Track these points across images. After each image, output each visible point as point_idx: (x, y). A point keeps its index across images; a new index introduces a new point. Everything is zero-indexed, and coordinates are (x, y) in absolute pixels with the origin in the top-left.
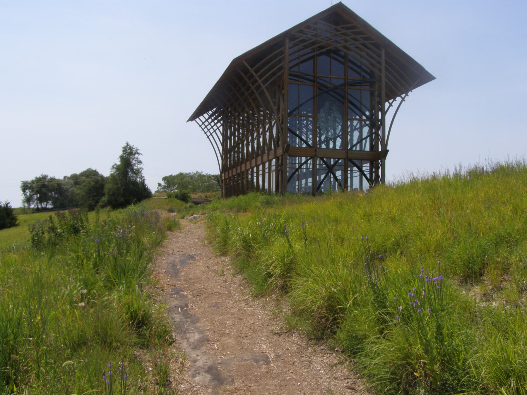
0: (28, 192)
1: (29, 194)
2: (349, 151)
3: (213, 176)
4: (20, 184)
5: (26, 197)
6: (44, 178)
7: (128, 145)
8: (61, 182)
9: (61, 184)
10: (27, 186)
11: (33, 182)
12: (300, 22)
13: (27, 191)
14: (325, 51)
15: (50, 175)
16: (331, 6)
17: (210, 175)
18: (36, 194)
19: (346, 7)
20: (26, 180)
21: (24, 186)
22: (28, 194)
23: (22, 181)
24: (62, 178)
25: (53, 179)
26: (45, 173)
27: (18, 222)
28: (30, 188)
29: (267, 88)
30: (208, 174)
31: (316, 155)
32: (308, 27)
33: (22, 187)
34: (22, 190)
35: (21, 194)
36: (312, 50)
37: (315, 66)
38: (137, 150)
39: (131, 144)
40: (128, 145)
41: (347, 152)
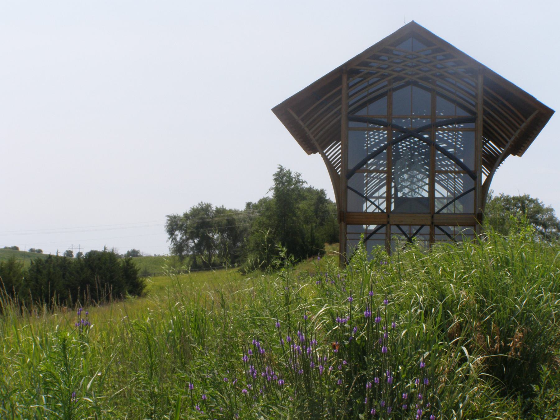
0: (179, 235)
1: (181, 239)
2: (435, 216)
3: (514, 198)
4: (164, 222)
5: (175, 244)
6: (206, 209)
7: (281, 169)
8: (235, 217)
9: (234, 220)
10: (177, 225)
11: (186, 216)
12: (357, 54)
13: (177, 232)
14: (403, 84)
15: (215, 204)
16: (404, 25)
17: (508, 196)
18: (192, 238)
19: (286, 100)
20: (175, 214)
21: (171, 225)
22: (178, 239)
23: (168, 216)
24: (242, 207)
25: (220, 211)
26: (206, 201)
27: (144, 291)
28: (180, 228)
29: (317, 141)
30: (505, 195)
31: (388, 222)
32: (366, 64)
33: (169, 226)
34: (168, 231)
35: (167, 239)
36: (443, 58)
37: (390, 105)
38: (298, 176)
39: (286, 168)
40: (281, 169)
41: (432, 217)
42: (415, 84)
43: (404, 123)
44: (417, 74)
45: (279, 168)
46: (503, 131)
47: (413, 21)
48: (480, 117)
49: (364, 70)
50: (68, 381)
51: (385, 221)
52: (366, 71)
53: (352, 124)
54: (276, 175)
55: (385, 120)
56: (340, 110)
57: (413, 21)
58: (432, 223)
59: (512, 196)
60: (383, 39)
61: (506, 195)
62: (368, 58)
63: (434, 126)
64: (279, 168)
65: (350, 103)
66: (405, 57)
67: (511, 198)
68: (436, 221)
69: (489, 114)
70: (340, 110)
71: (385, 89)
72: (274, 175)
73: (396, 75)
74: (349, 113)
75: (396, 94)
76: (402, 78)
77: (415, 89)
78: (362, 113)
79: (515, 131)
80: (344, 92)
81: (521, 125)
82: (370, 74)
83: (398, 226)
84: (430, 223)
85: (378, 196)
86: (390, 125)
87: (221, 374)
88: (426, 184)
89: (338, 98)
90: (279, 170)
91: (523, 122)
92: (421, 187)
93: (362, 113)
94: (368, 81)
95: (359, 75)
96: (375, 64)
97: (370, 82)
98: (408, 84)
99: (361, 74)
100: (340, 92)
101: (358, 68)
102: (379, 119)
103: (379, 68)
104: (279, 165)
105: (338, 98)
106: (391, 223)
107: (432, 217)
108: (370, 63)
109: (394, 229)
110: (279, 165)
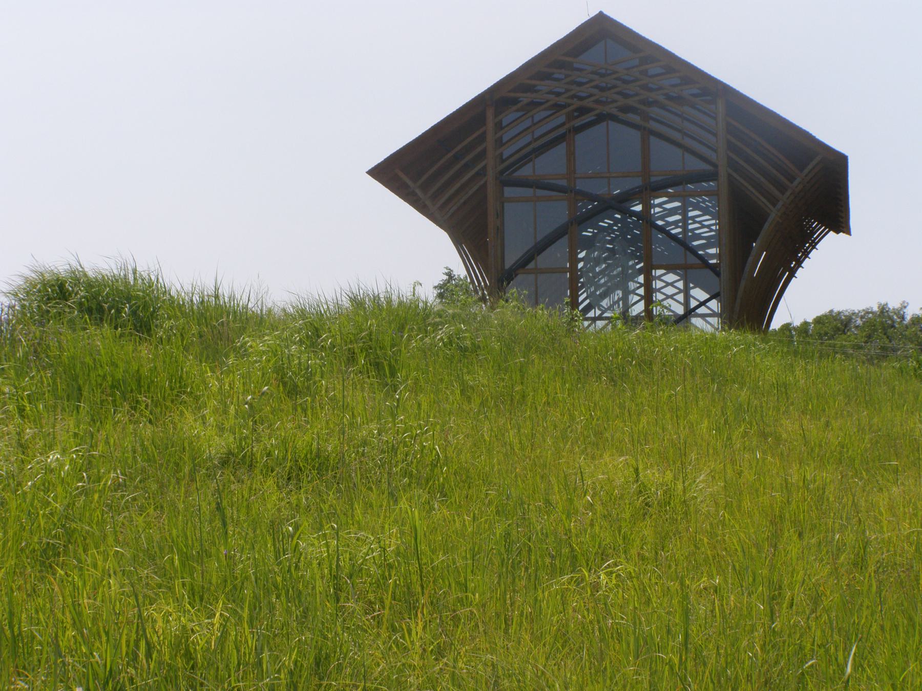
14: (593, 118)
16: (589, 18)
32: (561, 65)
37: (571, 155)
42: (612, 117)
43: (599, 189)
44: (614, 101)
45: (446, 274)
47: (601, 13)
48: (723, 171)
49: (525, 98)
52: (526, 101)
53: (509, 192)
54: (439, 287)
55: (563, 183)
57: (601, 13)
60: (501, 80)
62: (510, 92)
63: (646, 189)
64: (446, 274)
65: (506, 154)
66: (592, 73)
71: (562, 131)
72: (435, 287)
73: (577, 103)
74: (502, 172)
75: (579, 138)
76: (588, 110)
77: (613, 125)
78: (526, 172)
80: (490, 137)
82: (534, 104)
85: (593, 316)
86: (571, 191)
89: (479, 149)
90: (446, 277)
92: (671, 297)
93: (526, 172)
94: (532, 117)
95: (515, 108)
96: (544, 86)
97: (537, 119)
98: (601, 118)
99: (519, 105)
100: (482, 138)
101: (513, 95)
102: (546, 181)
103: (550, 92)
104: (447, 268)
105: (479, 149)
108: (553, 74)
110: (447, 268)
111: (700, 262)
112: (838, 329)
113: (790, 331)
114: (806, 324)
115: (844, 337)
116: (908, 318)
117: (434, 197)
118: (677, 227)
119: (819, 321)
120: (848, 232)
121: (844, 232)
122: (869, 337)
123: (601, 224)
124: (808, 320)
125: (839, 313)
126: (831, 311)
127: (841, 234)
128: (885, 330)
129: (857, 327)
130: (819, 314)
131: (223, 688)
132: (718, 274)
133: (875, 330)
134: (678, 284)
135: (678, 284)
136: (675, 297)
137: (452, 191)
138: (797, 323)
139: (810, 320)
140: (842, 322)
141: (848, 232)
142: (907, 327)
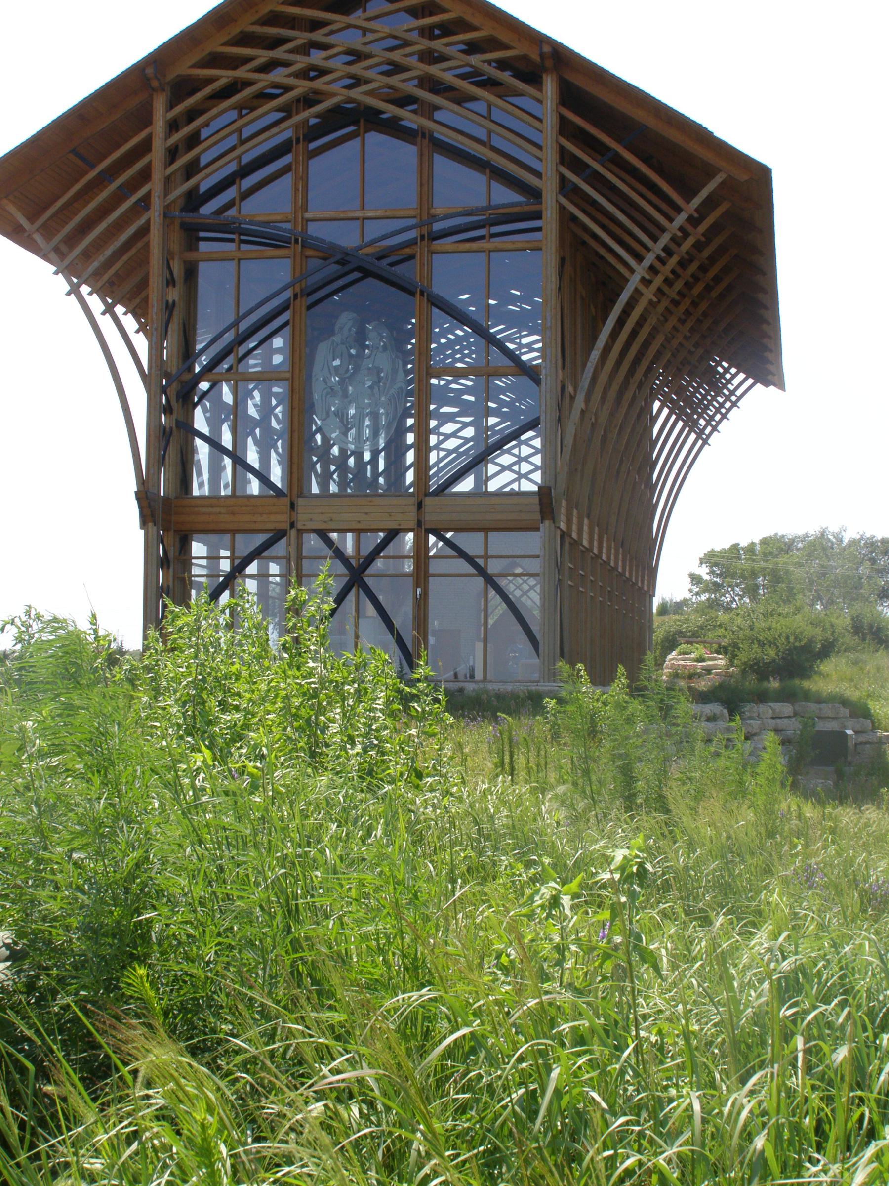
31: (292, 525)
46: (621, 242)
50: (608, 1116)
51: (281, 520)
56: (148, 195)
58: (419, 524)
59: (879, 539)
61: (868, 536)
67: (876, 541)
68: (431, 517)
69: (576, 189)
70: (148, 195)
79: (655, 239)
81: (671, 220)
83: (323, 534)
84: (413, 524)
87: (588, 1057)
88: (537, 468)
91: (679, 210)
106: (300, 526)
107: (420, 505)
109: (312, 541)
111: (513, 364)
112: (782, 550)
113: (738, 551)
114: (753, 544)
115: (787, 556)
116: (846, 541)
117: (71, 240)
118: (532, 350)
119: (764, 542)
120: (781, 385)
121: (775, 385)
122: (809, 555)
123: (502, 397)
124: (754, 541)
125: (783, 536)
126: (776, 534)
127: (772, 388)
128: (824, 549)
129: (798, 549)
130: (765, 536)
131: (3, 999)
132: (538, 382)
133: (816, 550)
134: (534, 443)
135: (534, 443)
136: (530, 459)
137: (124, 237)
138: (744, 543)
139: (757, 541)
140: (785, 544)
141: (781, 385)
142: (844, 549)
